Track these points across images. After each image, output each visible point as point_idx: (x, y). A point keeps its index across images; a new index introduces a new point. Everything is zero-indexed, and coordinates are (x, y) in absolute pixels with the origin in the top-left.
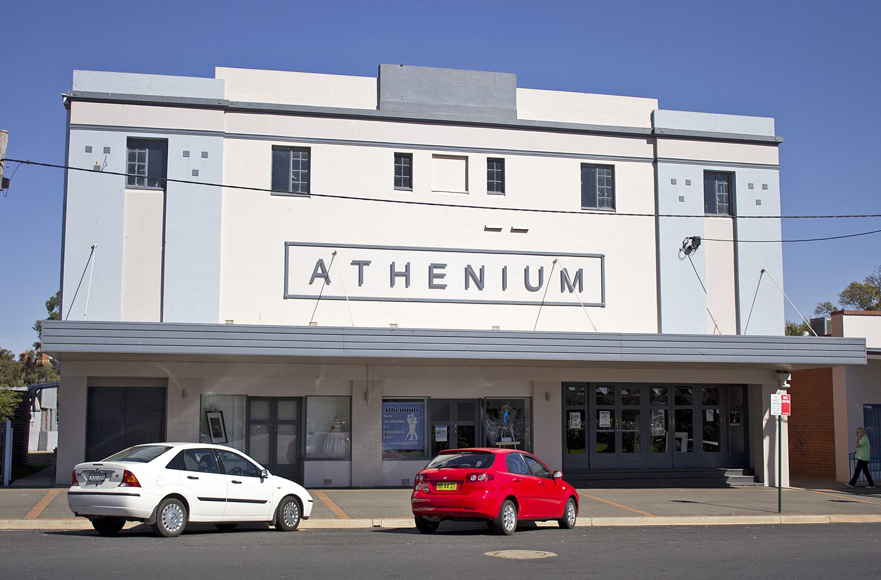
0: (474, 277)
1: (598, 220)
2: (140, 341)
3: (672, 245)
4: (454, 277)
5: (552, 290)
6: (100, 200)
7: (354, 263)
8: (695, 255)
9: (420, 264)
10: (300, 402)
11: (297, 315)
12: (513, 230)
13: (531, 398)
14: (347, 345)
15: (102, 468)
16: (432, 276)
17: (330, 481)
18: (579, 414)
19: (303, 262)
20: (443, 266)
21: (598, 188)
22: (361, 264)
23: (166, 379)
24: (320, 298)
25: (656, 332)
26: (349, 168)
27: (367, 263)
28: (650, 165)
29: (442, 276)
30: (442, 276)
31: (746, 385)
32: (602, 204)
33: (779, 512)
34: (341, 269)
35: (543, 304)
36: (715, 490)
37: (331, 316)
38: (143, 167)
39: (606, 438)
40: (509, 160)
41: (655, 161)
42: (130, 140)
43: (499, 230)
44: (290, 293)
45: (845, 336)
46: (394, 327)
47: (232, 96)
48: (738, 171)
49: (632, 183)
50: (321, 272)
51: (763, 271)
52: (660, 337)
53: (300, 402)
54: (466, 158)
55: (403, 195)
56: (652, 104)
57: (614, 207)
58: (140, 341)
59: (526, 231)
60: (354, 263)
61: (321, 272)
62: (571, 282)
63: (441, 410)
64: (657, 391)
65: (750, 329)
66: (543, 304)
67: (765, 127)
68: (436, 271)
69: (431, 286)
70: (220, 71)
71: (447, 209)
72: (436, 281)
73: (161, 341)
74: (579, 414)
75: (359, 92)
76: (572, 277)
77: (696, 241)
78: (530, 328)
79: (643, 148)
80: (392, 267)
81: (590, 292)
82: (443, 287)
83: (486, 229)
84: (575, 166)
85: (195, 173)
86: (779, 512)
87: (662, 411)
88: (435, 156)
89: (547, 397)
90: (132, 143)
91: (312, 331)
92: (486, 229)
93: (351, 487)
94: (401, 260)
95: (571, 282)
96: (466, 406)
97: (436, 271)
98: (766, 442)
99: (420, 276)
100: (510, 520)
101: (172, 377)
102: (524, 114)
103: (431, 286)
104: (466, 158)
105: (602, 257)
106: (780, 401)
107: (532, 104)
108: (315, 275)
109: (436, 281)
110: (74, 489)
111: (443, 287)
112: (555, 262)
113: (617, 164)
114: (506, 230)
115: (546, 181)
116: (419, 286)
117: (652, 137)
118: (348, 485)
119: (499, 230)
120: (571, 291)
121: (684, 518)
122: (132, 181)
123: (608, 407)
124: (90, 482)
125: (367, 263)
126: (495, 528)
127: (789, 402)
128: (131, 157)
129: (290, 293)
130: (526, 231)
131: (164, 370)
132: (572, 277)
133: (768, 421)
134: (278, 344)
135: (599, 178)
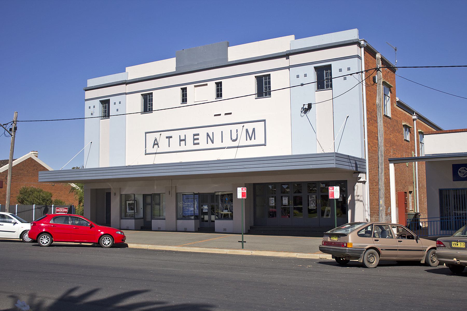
2: (60, 177)
4: (202, 139)
5: (243, 141)
6: (94, 126)
7: (167, 137)
8: (310, 113)
9: (190, 134)
12: (226, 114)
16: (194, 139)
18: (274, 198)
20: (198, 135)
21: (263, 87)
23: (110, 189)
24: (156, 153)
26: (165, 98)
27: (171, 137)
29: (198, 139)
30: (198, 139)
32: (327, 87)
33: (243, 248)
34: (163, 141)
35: (238, 147)
36: (309, 238)
38: (326, 82)
39: (285, 210)
40: (223, 81)
43: (220, 115)
47: (130, 78)
48: (333, 63)
50: (156, 143)
58: (60, 177)
59: (231, 113)
60: (167, 137)
61: (156, 143)
63: (202, 198)
64: (270, 187)
66: (238, 147)
67: (352, 34)
69: (194, 144)
70: (128, 69)
71: (202, 108)
72: (196, 142)
74: (274, 198)
75: (170, 65)
76: (250, 133)
77: (310, 106)
78: (152, 163)
81: (259, 139)
82: (198, 144)
85: (92, 114)
86: (243, 248)
87: (314, 196)
88: (195, 86)
96: (213, 196)
98: (349, 212)
99: (190, 140)
100: (107, 242)
101: (112, 188)
102: (231, 58)
106: (241, 191)
108: (154, 144)
109: (196, 142)
111: (198, 144)
112: (243, 126)
113: (333, 63)
114: (223, 114)
116: (190, 145)
118: (175, 230)
119: (220, 115)
120: (251, 140)
121: (184, 248)
123: (287, 195)
125: (171, 137)
126: (98, 245)
127: (245, 191)
130: (231, 113)
131: (109, 185)
132: (250, 133)
133: (350, 201)
135: (265, 82)
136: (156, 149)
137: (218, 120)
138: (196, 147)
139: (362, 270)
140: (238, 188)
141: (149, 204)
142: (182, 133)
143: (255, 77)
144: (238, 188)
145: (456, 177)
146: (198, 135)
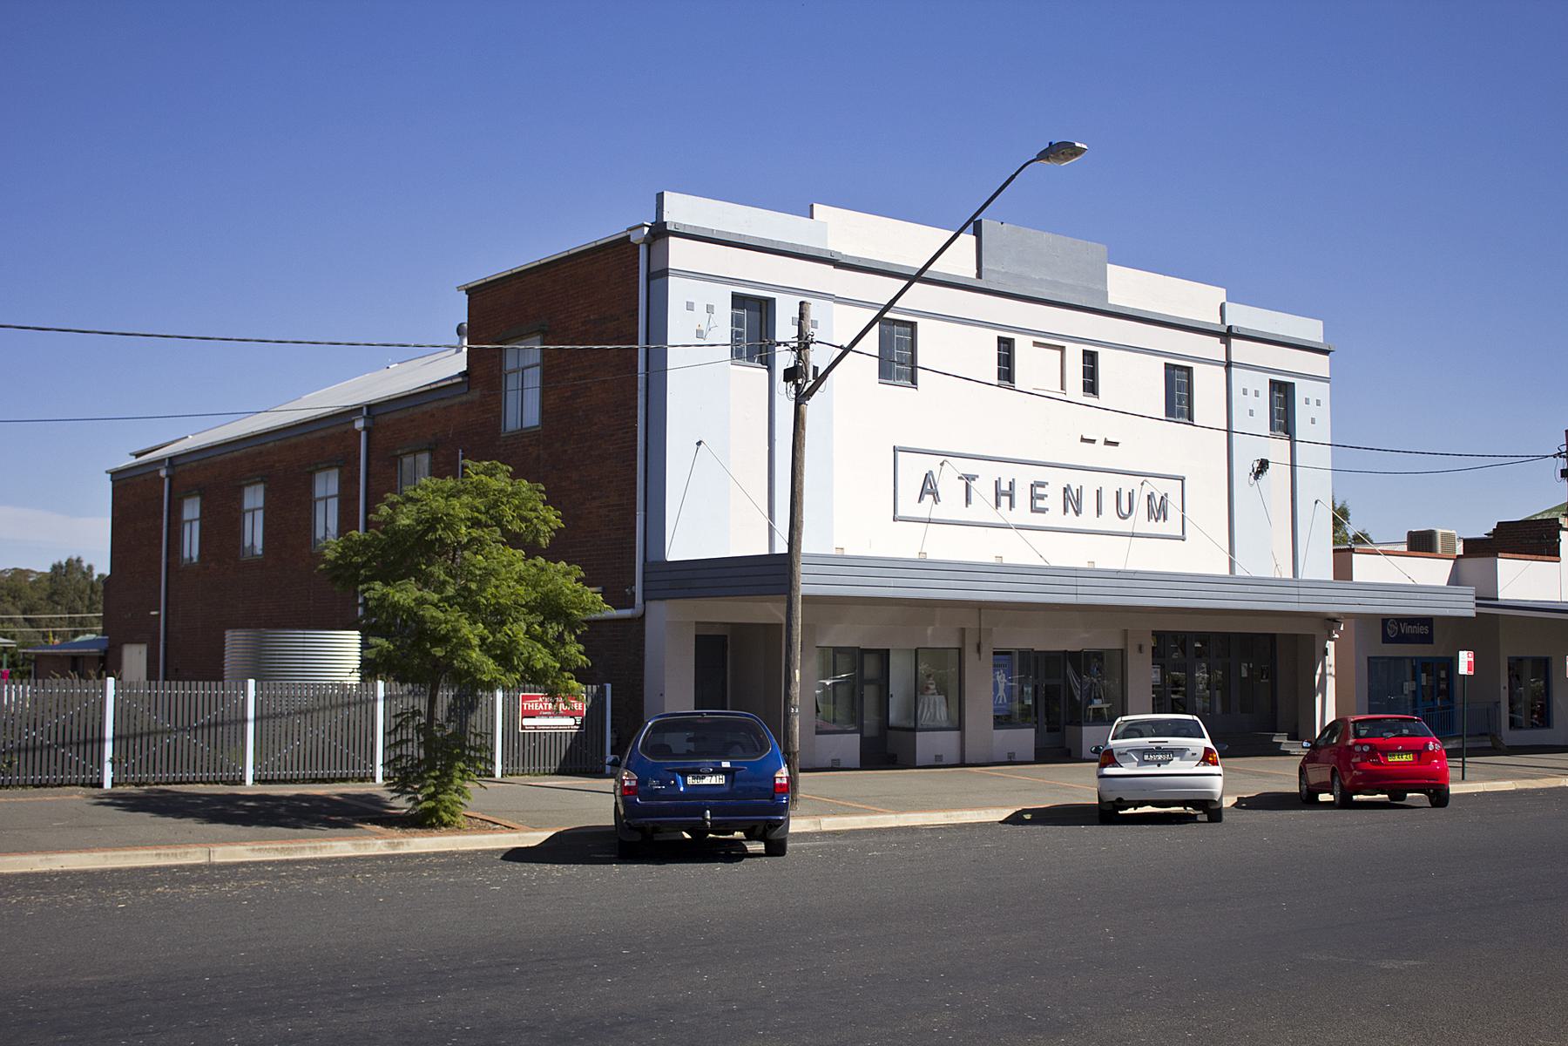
0: (1072, 501)
1: (1178, 429)
3: (1243, 468)
8: (1263, 478)
10: (884, 655)
11: (903, 544)
13: (1123, 652)
14: (1080, 589)
15: (1163, 746)
17: (939, 757)
19: (913, 470)
20: (1042, 485)
21: (1179, 397)
22: (969, 479)
25: (1226, 572)
27: (974, 478)
28: (1222, 369)
29: (1042, 497)
30: (1042, 497)
31: (1274, 635)
32: (1181, 414)
37: (1017, 550)
41: (1228, 365)
42: (735, 296)
43: (1093, 441)
44: (900, 513)
45: (1355, 579)
46: (839, 553)
49: (1207, 386)
50: (929, 488)
51: (699, 443)
52: (1232, 580)
53: (884, 655)
54: (1062, 349)
55: (1091, 400)
56: (1219, 294)
57: (1191, 418)
59: (1116, 444)
61: (929, 488)
62: (1158, 510)
65: (1305, 574)
67: (1312, 330)
68: (1039, 491)
69: (1034, 510)
72: (1039, 504)
73: (1135, 592)
79: (1214, 348)
80: (997, 483)
82: (1043, 511)
83: (1083, 440)
84: (1157, 367)
85: (699, 334)
88: (1036, 344)
89: (1140, 648)
90: (738, 301)
91: (923, 566)
92: (1083, 440)
93: (962, 764)
94: (1006, 473)
95: (1158, 510)
97: (1039, 491)
98: (1318, 700)
103: (1034, 510)
104: (1062, 349)
105: (1183, 479)
107: (1127, 286)
109: (1039, 504)
110: (1108, 771)
111: (1043, 511)
113: (1017, 337)
114: (1100, 442)
115: (1134, 380)
117: (1227, 335)
118: (956, 761)
122: (737, 354)
124: (1143, 762)
125: (974, 478)
128: (736, 321)
129: (900, 513)
134: (1215, 595)
136: (926, 508)
137: (1089, 455)
138: (1038, 519)
139: (1197, 835)
140: (228, 634)
141: (870, 682)
142: (1006, 473)
143: (1271, 382)
144: (228, 634)
145: (1386, 639)
146: (1042, 485)
